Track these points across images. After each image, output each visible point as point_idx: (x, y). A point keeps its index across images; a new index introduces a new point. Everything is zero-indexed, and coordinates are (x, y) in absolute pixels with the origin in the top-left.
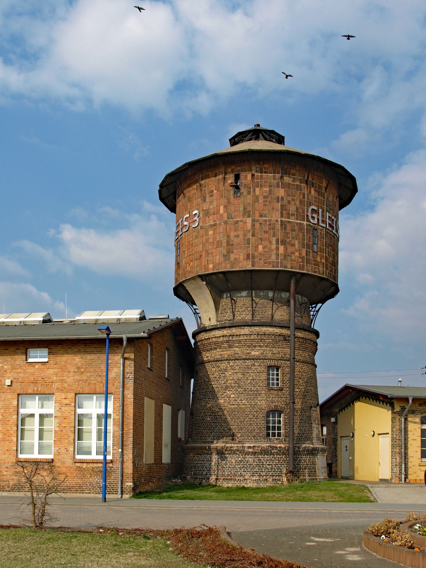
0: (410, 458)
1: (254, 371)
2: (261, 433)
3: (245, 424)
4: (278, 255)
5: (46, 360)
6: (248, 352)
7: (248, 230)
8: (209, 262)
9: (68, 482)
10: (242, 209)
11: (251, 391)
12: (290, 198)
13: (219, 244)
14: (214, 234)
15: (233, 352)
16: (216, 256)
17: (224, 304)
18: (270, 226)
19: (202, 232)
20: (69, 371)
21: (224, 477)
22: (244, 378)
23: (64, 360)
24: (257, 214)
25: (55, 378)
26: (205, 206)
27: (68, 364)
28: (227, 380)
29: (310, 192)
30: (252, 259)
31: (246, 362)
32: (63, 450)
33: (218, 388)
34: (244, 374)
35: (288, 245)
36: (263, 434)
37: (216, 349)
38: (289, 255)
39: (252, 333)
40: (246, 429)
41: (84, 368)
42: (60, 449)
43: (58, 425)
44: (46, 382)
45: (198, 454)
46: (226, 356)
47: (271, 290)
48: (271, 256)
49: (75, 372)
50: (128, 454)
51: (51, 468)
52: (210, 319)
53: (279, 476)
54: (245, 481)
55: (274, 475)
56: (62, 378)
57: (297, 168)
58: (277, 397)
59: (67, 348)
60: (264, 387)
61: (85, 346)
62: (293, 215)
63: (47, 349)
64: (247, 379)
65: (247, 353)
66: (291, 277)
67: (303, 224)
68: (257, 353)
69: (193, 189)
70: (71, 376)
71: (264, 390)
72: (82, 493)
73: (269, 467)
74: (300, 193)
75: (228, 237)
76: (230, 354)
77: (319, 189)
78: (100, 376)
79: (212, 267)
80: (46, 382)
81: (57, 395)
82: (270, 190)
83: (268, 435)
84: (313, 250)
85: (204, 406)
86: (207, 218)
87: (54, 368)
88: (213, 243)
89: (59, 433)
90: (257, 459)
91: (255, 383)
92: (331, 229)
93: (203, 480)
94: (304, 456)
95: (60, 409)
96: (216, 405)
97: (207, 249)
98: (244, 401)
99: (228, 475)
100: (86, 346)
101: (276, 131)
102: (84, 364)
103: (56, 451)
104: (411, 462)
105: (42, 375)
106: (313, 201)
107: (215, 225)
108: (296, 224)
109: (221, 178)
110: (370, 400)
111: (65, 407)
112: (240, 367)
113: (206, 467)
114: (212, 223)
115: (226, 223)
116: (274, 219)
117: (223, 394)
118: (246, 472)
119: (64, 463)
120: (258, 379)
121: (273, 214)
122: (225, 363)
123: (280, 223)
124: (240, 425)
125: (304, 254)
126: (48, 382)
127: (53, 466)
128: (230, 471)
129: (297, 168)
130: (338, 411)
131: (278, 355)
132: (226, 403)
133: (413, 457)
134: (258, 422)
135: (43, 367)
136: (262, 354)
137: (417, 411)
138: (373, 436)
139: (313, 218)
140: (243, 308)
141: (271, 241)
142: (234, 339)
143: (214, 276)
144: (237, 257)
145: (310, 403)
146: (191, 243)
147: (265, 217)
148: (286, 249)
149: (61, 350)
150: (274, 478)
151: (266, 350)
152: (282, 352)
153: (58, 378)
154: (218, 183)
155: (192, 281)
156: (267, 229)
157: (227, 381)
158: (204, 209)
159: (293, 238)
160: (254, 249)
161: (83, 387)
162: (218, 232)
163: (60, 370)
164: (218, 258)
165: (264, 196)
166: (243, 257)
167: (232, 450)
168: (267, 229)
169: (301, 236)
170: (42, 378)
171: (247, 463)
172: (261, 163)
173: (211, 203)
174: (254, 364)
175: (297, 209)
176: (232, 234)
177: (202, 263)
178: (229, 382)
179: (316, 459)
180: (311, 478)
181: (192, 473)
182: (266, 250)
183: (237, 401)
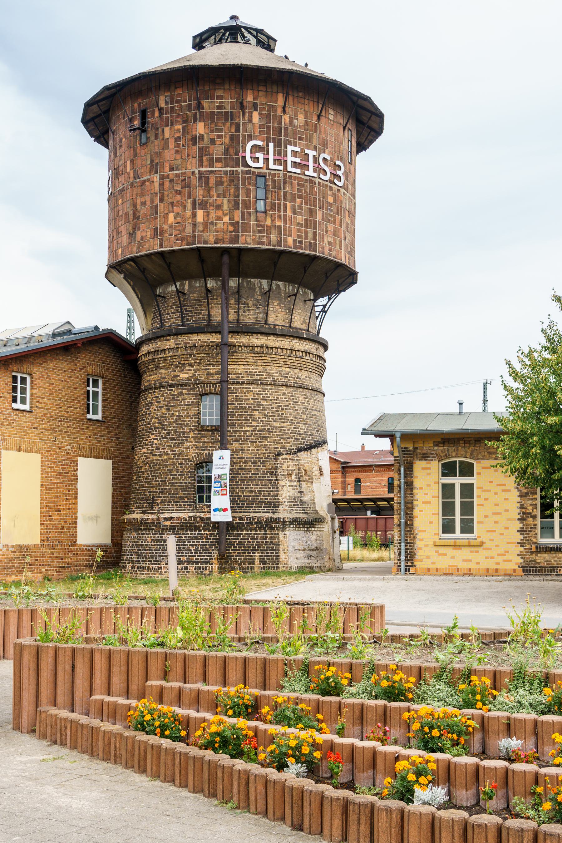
0: (420, 534)
1: (181, 402)
2: (187, 497)
3: (166, 483)
4: (194, 225)
6: (176, 374)
7: (156, 192)
10: (148, 162)
11: (176, 433)
12: (213, 136)
15: (160, 376)
18: (184, 182)
22: (169, 414)
24: (167, 168)
29: (250, 120)
30: (160, 235)
31: (172, 390)
34: (169, 409)
35: (212, 208)
36: (188, 499)
38: (212, 223)
39: (177, 346)
47: (210, 277)
48: (185, 229)
53: (207, 562)
57: (227, 87)
60: (193, 426)
62: (219, 160)
66: (222, 255)
68: (187, 376)
71: (193, 431)
73: (192, 549)
74: (231, 124)
75: (135, 206)
82: (184, 128)
91: (182, 421)
104: (422, 540)
108: (225, 174)
112: (165, 398)
116: (189, 171)
118: (162, 556)
120: (185, 416)
121: (189, 163)
123: (197, 176)
125: (237, 217)
129: (227, 87)
133: (425, 531)
134: (183, 480)
137: (432, 454)
139: (256, 160)
144: (144, 234)
148: (208, 214)
150: (199, 565)
156: (178, 187)
159: (218, 196)
160: (162, 220)
165: (176, 139)
168: (178, 187)
169: (232, 191)
172: (173, 88)
174: (181, 392)
175: (226, 150)
176: (139, 201)
178: (153, 421)
182: (179, 219)
183: (159, 449)
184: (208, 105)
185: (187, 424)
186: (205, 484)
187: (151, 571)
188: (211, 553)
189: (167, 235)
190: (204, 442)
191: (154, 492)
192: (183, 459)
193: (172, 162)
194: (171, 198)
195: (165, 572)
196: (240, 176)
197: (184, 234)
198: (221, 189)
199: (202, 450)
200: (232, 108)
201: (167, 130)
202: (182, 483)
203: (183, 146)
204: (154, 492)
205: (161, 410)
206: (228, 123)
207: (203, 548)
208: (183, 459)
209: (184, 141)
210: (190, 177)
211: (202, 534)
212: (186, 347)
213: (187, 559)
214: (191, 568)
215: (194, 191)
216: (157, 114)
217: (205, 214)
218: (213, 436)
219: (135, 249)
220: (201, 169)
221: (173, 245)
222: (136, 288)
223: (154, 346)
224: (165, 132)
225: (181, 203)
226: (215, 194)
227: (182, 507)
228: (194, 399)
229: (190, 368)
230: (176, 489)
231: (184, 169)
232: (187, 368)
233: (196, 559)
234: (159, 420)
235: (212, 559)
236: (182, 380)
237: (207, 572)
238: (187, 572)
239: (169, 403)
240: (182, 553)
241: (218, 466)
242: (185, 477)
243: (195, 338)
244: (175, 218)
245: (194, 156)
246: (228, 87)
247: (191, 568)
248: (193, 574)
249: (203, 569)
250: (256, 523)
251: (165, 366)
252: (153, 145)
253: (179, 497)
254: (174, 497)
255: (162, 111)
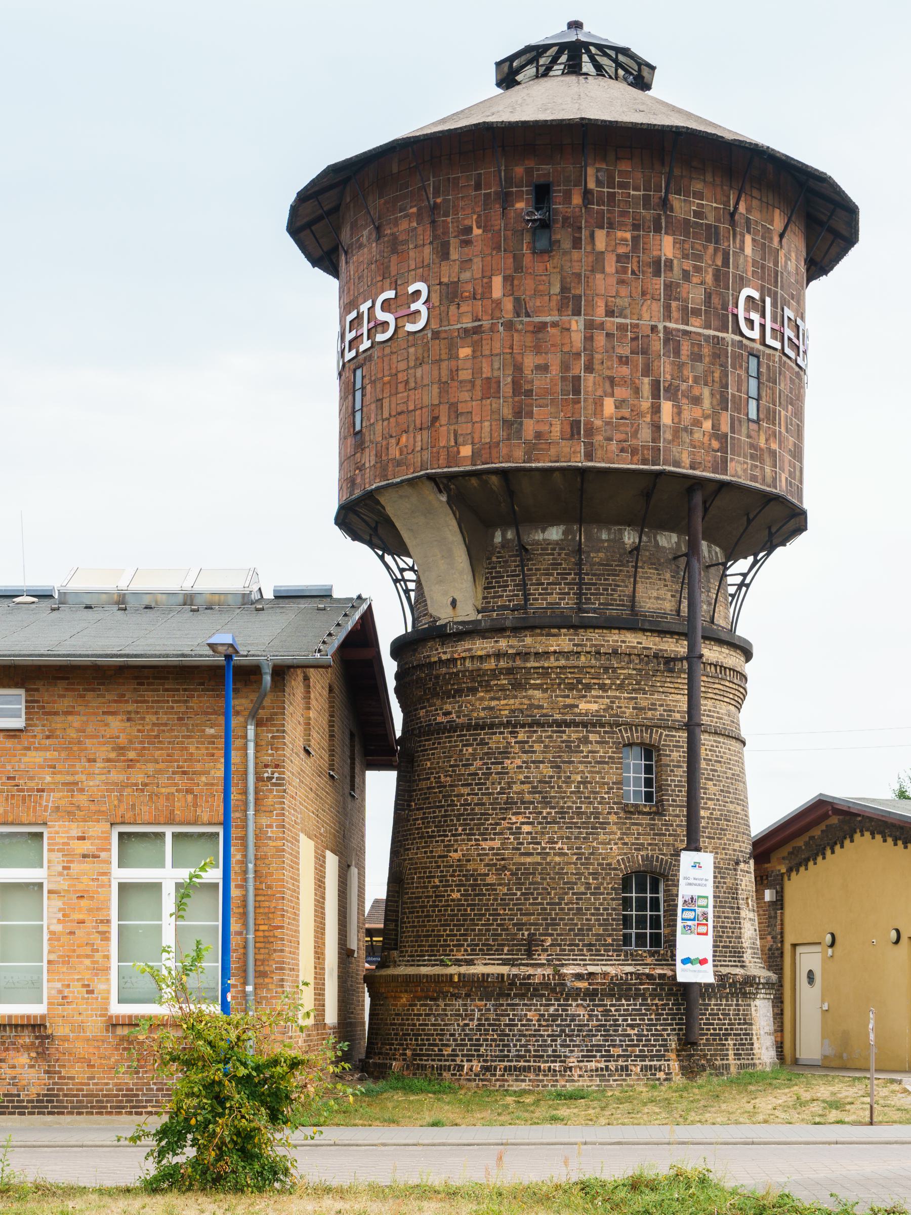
1: (587, 757)
2: (610, 935)
3: (563, 909)
4: (656, 427)
5: (18, 723)
6: (568, 701)
7: (574, 350)
8: (460, 440)
9: (95, 1084)
10: (556, 289)
11: (579, 814)
13: (491, 388)
14: (474, 357)
15: (526, 701)
16: (481, 422)
17: (494, 559)
18: (635, 343)
19: (437, 348)
20: (92, 757)
21: (506, 1063)
22: (559, 778)
23: (76, 724)
24: (601, 310)
25: (48, 779)
26: (448, 273)
27: (87, 737)
28: (508, 783)
29: (742, 249)
31: (564, 732)
32: (77, 990)
33: (484, 804)
34: (559, 767)
35: (685, 401)
36: (613, 940)
37: (473, 690)
39: (579, 649)
40: (566, 925)
41: (135, 749)
42: (68, 986)
43: (60, 916)
44: (22, 790)
45: (426, 998)
46: (507, 712)
47: (629, 526)
49: (108, 760)
50: (272, 997)
51: (42, 1044)
52: (454, 603)
53: (660, 1057)
54: (568, 1073)
55: (646, 1056)
56: (69, 779)
58: (649, 834)
59: (85, 690)
61: (138, 684)
62: (696, 312)
63: (21, 692)
64: (568, 781)
65: (565, 707)
67: (723, 339)
68: (594, 707)
69: (406, 216)
70: (97, 772)
72: (137, 1113)
73: (632, 1032)
75: (518, 368)
76: (517, 706)
77: (763, 237)
78: (184, 773)
79: (470, 454)
80: (22, 790)
81: (57, 829)
82: (635, 239)
83: (626, 940)
84: (747, 415)
85: (440, 857)
86: (453, 308)
87: (47, 749)
88: (472, 383)
89: (64, 939)
90: (600, 1009)
92: (792, 354)
93: (445, 1074)
94: (724, 1002)
95: (64, 868)
96: (479, 855)
97: (453, 400)
98: (559, 845)
99: (518, 1056)
100: (142, 684)
101: (635, 50)
102: (137, 737)
103: (54, 992)
105: (9, 768)
106: (750, 273)
107: (477, 330)
108: (706, 341)
109: (496, 193)
110: (885, 841)
111: (79, 862)
112: (545, 747)
113: (451, 1035)
114: (470, 325)
115: (509, 326)
117: (497, 824)
118: (569, 1046)
119: (81, 1027)
120: (597, 783)
121: (645, 308)
122: (501, 733)
123: (661, 335)
124: (550, 914)
125: (725, 427)
126: (28, 790)
127: (48, 1037)
128: (526, 1046)
129: (709, 178)
130: (784, 870)
131: (650, 714)
132: (507, 849)
134: (601, 904)
135: (9, 743)
136: (609, 708)
138: (897, 942)
139: (750, 323)
140: (552, 574)
141: (638, 388)
142: (528, 665)
143: (474, 481)
144: (544, 428)
145: (735, 850)
146: (402, 377)
147: (620, 316)
148: (678, 412)
149: (64, 696)
150: (648, 1063)
151: (619, 698)
152: (661, 705)
153: (59, 778)
154: (486, 206)
155: (407, 490)
156: (625, 350)
157: (510, 785)
158: (445, 280)
159: (696, 380)
160: (591, 407)
161: (133, 806)
162: (487, 352)
163: (64, 755)
164: (486, 431)
166: (562, 432)
167: (530, 984)
168: (625, 350)
169: (717, 375)
170: (9, 778)
171: (572, 1021)
173: (466, 263)
175: (708, 296)
176: (530, 361)
177: (437, 439)
178: (516, 788)
179: (753, 1009)
180: (742, 1061)
181: (408, 1052)
183: (539, 843)
184: (681, 207)
185: (602, 798)
186: (634, 913)
187: (545, 1075)
188: (666, 1040)
189: (600, 438)
190: (639, 834)
191: (531, 924)
192: (599, 864)
193: (610, 299)
194: (608, 369)
195: (580, 1076)
196: (730, 349)
197: (634, 442)
198: (700, 367)
199: (635, 849)
200: (717, 220)
201: (601, 236)
202: (598, 909)
203: (633, 273)
204: (531, 924)
205: (538, 767)
206: (711, 247)
207: (651, 1030)
208: (599, 864)
209: (635, 264)
210: (648, 336)
211: (647, 1005)
212: (599, 653)
213: (623, 1051)
214: (633, 1068)
215: (656, 363)
216: (577, 200)
217: (675, 410)
218: (654, 825)
219: (519, 453)
220: (668, 324)
221: (612, 458)
222: (463, 525)
223: (514, 642)
224: (596, 239)
225: (629, 382)
226: (691, 375)
227: (603, 955)
228: (614, 752)
229: (601, 693)
230: (587, 920)
231: (635, 317)
232: (593, 693)
233: (641, 1051)
234: (533, 787)
235: (667, 1051)
236: (586, 715)
237: (661, 1075)
238: (627, 1075)
239: (559, 757)
240: (612, 1040)
241: (691, 881)
242: (604, 899)
243: (616, 638)
244: (616, 407)
245: (656, 297)
246: (711, 180)
247: (633, 1068)
248: (638, 1080)
249: (656, 1070)
250: (731, 985)
251: (542, 684)
252: (567, 258)
253: (593, 935)
254: (583, 935)
255: (590, 196)
